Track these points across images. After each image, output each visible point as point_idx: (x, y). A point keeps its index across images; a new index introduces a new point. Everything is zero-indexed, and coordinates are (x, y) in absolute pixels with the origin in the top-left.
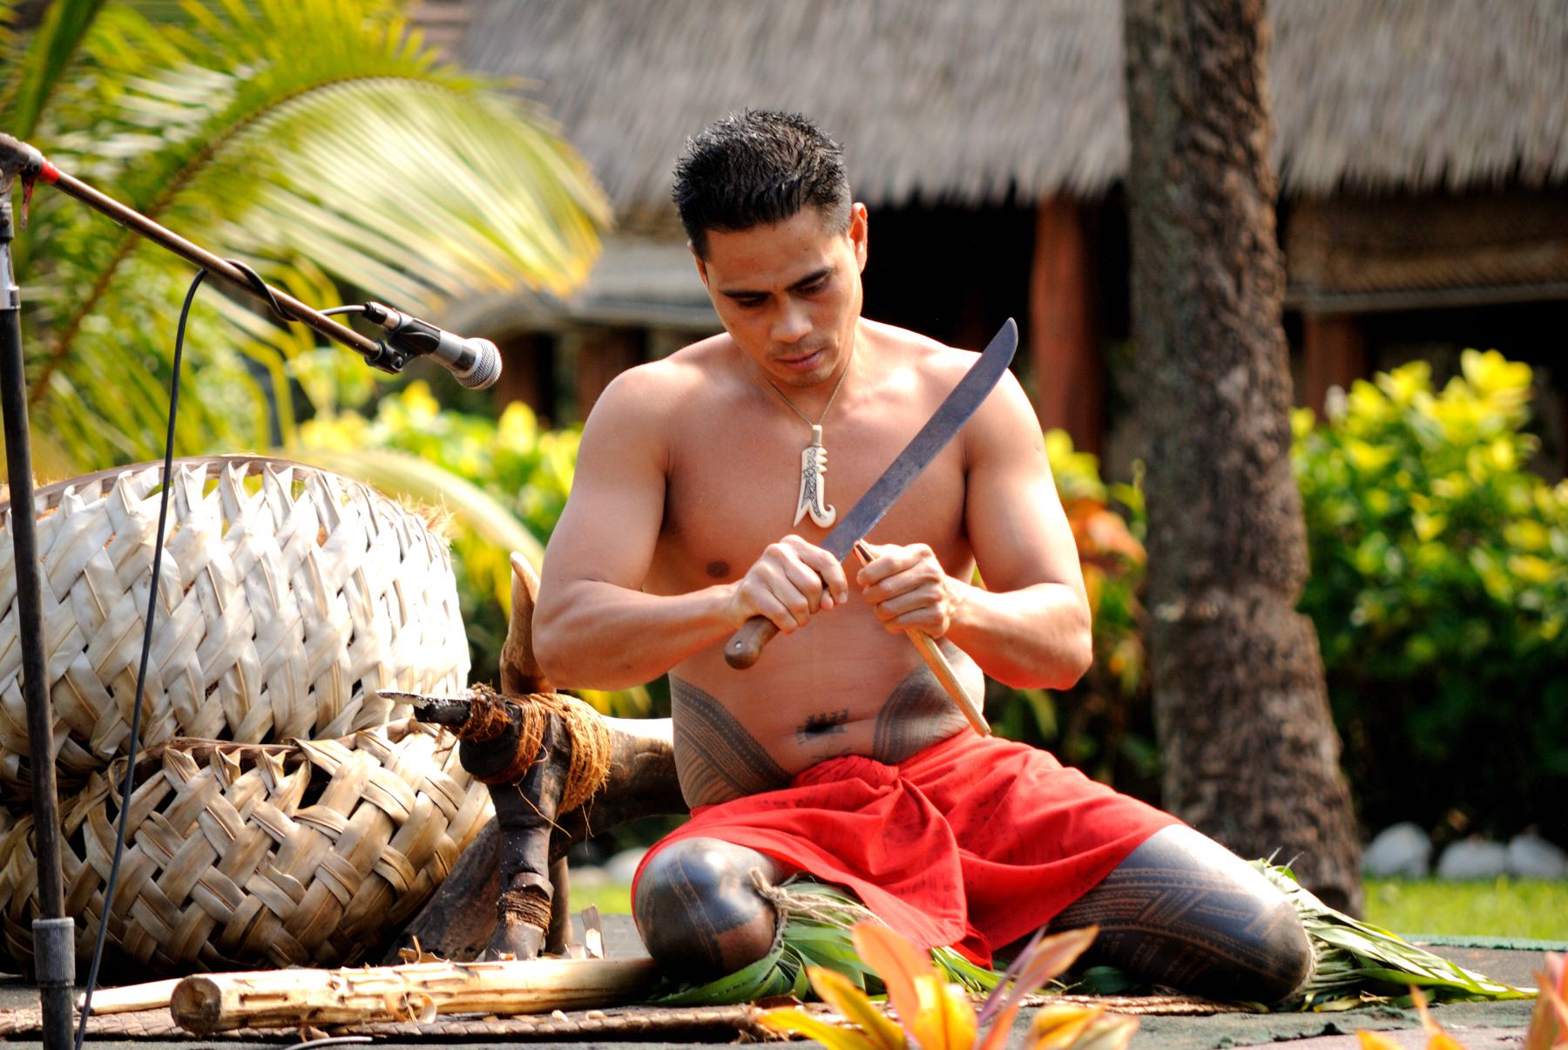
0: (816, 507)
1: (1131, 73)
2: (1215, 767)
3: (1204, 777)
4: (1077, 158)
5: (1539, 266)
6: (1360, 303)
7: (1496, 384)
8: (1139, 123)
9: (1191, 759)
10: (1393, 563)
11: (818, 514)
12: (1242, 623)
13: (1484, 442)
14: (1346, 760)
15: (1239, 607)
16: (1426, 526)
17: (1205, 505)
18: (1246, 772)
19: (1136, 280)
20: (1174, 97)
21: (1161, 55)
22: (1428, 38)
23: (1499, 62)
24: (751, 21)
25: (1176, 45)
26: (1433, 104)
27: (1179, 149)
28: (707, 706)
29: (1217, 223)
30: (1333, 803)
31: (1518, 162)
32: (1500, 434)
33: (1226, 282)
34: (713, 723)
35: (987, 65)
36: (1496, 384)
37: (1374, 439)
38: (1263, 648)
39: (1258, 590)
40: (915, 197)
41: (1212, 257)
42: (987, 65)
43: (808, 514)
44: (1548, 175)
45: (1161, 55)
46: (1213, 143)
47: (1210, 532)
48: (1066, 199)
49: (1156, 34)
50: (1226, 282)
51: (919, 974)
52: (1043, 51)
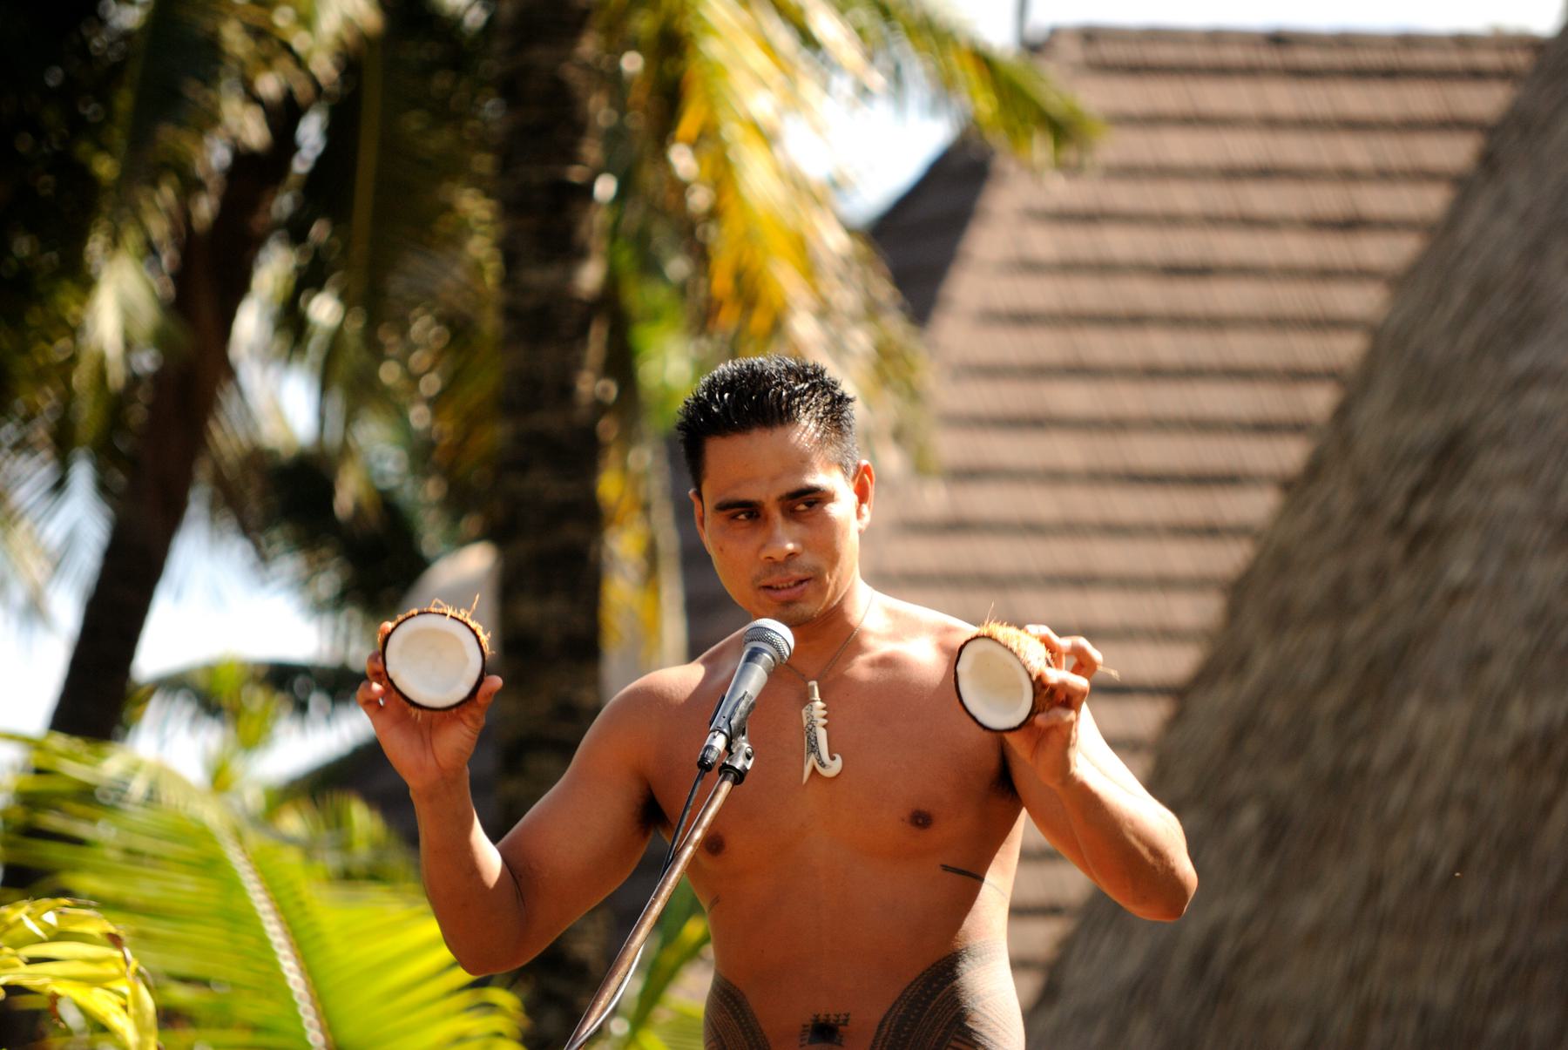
0: (819, 759)
11: (823, 765)
43: (814, 768)
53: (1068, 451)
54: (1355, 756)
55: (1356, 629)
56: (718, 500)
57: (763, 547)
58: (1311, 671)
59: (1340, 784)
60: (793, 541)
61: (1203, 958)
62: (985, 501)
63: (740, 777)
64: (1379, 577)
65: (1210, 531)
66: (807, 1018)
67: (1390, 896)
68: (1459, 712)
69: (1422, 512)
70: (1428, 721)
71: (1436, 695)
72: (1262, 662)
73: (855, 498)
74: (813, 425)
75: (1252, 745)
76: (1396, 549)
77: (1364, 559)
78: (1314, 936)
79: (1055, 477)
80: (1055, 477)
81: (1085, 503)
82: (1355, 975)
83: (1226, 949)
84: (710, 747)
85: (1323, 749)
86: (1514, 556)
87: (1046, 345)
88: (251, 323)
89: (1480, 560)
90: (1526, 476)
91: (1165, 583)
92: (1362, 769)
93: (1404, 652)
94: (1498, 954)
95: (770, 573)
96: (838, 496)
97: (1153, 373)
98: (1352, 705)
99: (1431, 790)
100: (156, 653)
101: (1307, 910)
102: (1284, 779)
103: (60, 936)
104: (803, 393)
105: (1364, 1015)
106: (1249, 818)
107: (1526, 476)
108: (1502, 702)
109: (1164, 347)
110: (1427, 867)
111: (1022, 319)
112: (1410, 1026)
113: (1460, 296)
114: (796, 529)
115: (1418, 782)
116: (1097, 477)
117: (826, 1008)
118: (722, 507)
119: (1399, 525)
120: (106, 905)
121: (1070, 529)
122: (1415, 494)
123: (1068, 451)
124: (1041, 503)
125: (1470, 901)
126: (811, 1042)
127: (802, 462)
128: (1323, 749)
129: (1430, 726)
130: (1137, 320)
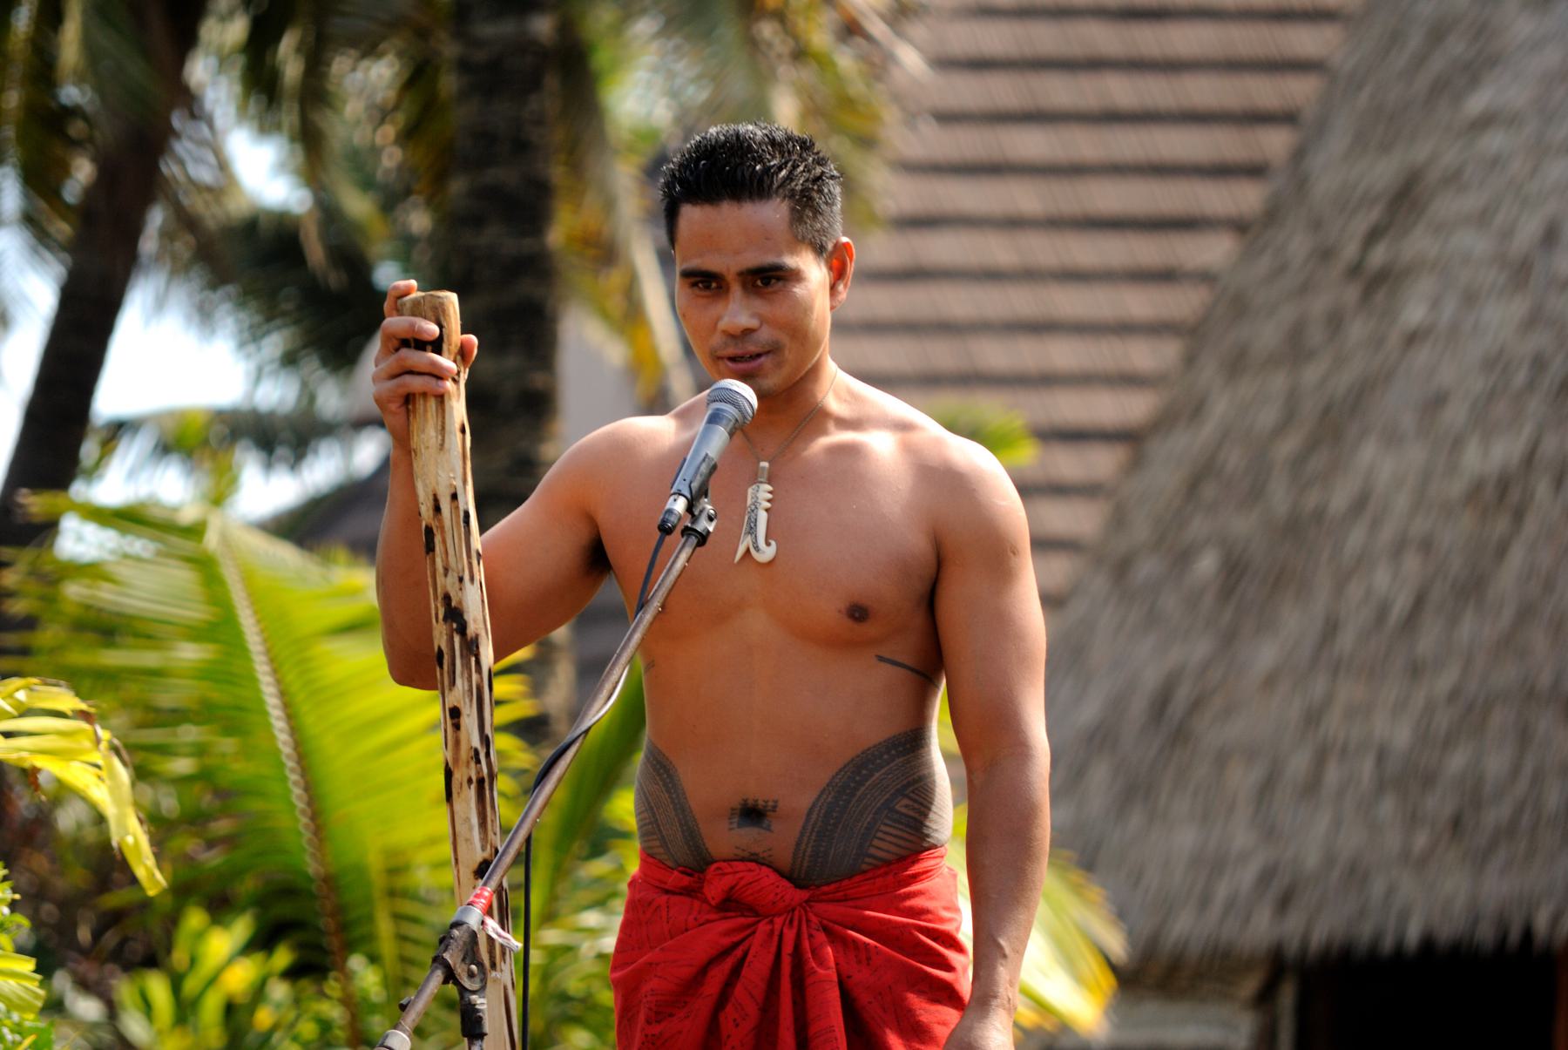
0: (755, 543)
11: (757, 549)
24: (1256, 774)
28: (664, 767)
34: (665, 785)
40: (1428, 944)
42: (1496, 815)
43: (748, 551)
53: (1026, 198)
54: (1312, 499)
55: (1312, 374)
58: (1268, 417)
59: (1296, 529)
61: (1161, 702)
62: (942, 248)
63: (703, 538)
64: (1335, 322)
65: (1166, 276)
66: (736, 802)
67: (1346, 640)
68: (1416, 455)
69: (1378, 256)
70: (1381, 463)
71: (1392, 438)
72: (1220, 407)
75: (1209, 491)
76: (1352, 294)
77: (1318, 306)
78: (1270, 682)
79: (1013, 223)
80: (1013, 223)
81: (1044, 250)
82: (1313, 718)
83: (1183, 695)
84: (670, 511)
85: (1279, 497)
86: (1471, 299)
87: (1002, 91)
88: (211, 76)
89: (1435, 304)
90: (1482, 218)
91: (1124, 329)
92: (1319, 515)
93: (1362, 393)
94: (1454, 695)
97: (1112, 117)
98: (1312, 445)
99: (1387, 533)
101: (1265, 655)
102: (1242, 525)
103: (27, 712)
105: (1320, 758)
106: (1207, 564)
107: (1482, 218)
108: (1457, 444)
109: (1121, 91)
111: (980, 65)
112: (1367, 766)
113: (1415, 40)
115: (1375, 524)
116: (1055, 223)
117: (756, 792)
119: (1355, 270)
120: (74, 679)
121: (1029, 275)
122: (1373, 236)
123: (1026, 198)
124: (999, 250)
125: (1427, 641)
126: (739, 826)
128: (1279, 497)
129: (1387, 469)
130: (1096, 64)
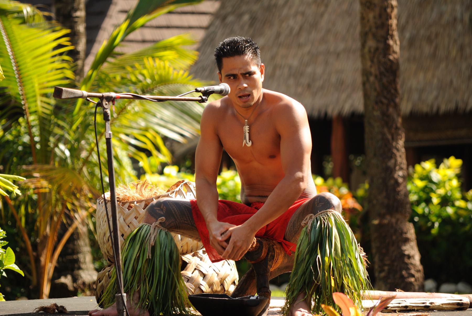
1: (364, 84)
2: (387, 262)
3: (385, 265)
4: (343, 107)
5: (462, 134)
6: (416, 144)
7: (453, 164)
8: (366, 96)
9: (381, 260)
10: (427, 210)
12: (394, 225)
13: (450, 180)
14: (422, 261)
15: (394, 220)
16: (435, 200)
17: (384, 194)
18: (396, 264)
19: (366, 136)
20: (375, 90)
21: (372, 79)
22: (433, 76)
23: (451, 82)
25: (376, 76)
26: (435, 93)
27: (376, 103)
29: (387, 121)
30: (418, 271)
31: (457, 108)
32: (454, 178)
33: (389, 137)
35: (318, 84)
36: (453, 164)
37: (422, 179)
38: (400, 231)
39: (399, 216)
41: (386, 130)
42: (318, 84)
44: (465, 110)
45: (372, 79)
46: (385, 101)
47: (386, 201)
48: (340, 116)
49: (371, 74)
50: (389, 137)
51: (351, 307)
52: (333, 79)
56: (226, 74)
57: (238, 86)
60: (246, 84)
67: (282, 38)
73: (260, 73)
74: (250, 55)
94: (309, 52)
95: (240, 92)
96: (256, 73)
99: (293, 11)
100: (94, 126)
104: (247, 47)
106: (246, 18)
110: (291, 31)
114: (247, 81)
118: (227, 76)
125: (302, 39)
127: (247, 64)
